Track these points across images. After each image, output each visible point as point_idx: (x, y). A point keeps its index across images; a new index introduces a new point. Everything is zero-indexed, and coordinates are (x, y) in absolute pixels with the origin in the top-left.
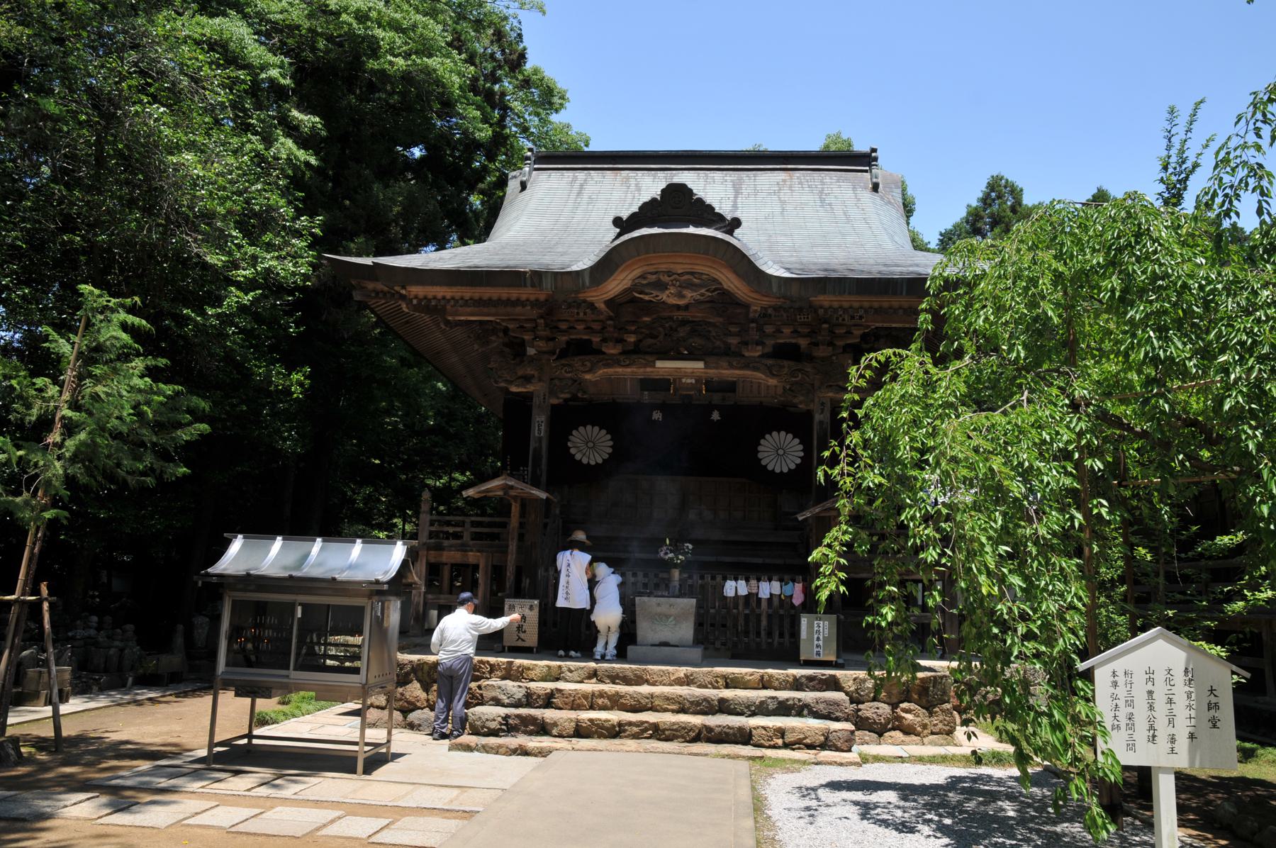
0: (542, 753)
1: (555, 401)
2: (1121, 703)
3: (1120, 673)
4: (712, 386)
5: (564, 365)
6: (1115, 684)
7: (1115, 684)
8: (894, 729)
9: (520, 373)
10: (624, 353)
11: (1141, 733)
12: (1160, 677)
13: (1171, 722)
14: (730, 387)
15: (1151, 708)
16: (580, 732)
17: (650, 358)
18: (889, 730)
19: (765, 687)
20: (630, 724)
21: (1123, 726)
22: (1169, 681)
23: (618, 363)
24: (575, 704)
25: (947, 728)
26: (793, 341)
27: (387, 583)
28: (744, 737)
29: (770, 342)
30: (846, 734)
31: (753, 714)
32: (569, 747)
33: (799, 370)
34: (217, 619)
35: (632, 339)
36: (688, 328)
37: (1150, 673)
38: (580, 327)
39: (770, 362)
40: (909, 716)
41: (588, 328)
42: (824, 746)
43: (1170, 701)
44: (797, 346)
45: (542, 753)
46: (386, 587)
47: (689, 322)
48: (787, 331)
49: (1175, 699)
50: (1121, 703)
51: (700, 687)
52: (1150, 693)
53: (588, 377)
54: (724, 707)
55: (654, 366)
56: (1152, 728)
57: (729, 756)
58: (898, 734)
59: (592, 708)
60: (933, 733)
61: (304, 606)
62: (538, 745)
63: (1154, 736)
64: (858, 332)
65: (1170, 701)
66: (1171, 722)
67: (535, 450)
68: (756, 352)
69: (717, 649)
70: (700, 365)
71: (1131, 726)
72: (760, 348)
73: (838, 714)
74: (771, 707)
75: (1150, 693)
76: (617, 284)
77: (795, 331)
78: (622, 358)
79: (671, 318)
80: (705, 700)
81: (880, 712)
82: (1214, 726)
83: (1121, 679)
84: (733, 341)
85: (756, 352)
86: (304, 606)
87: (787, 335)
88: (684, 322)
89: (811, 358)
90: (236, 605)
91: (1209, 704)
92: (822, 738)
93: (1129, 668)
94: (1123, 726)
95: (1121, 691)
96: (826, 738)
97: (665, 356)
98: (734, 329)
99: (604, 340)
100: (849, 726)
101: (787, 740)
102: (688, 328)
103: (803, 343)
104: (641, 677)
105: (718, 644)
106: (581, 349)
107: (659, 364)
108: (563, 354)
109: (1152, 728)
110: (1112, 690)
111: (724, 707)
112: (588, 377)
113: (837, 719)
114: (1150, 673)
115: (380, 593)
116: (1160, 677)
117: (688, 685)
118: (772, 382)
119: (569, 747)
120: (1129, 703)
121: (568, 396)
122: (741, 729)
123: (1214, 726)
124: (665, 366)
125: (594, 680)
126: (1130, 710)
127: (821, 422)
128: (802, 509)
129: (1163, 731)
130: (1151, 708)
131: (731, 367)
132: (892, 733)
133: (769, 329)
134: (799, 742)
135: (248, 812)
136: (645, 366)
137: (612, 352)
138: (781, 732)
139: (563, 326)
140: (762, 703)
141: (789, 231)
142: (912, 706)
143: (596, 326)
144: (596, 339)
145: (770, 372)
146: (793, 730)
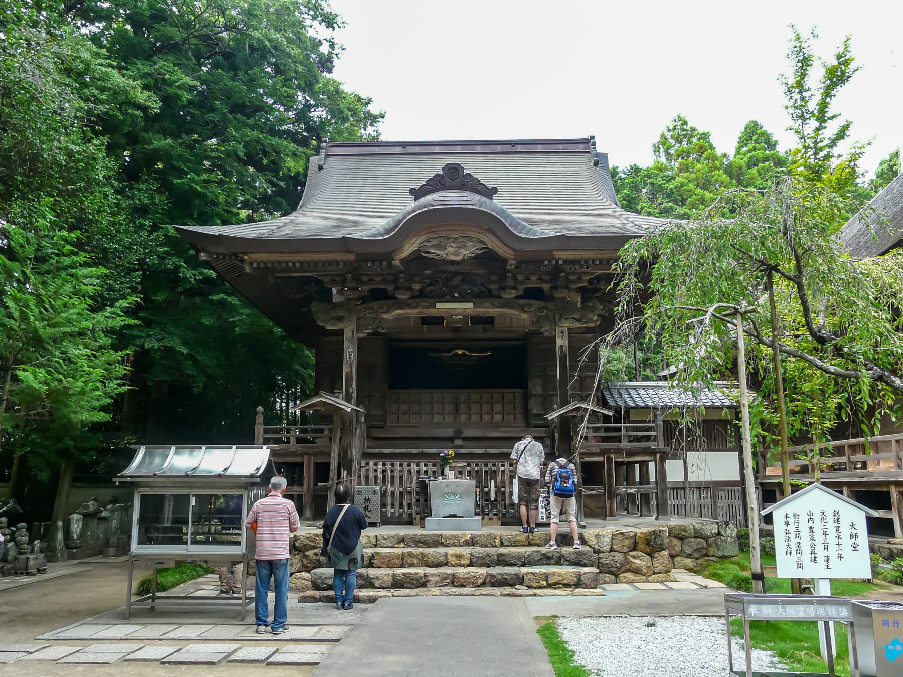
0: (372, 600)
1: (362, 336)
2: (792, 536)
3: (791, 515)
4: (477, 320)
5: (367, 308)
6: (787, 523)
7: (787, 523)
8: (627, 571)
9: (334, 315)
10: (412, 298)
11: (806, 556)
12: (817, 517)
13: (826, 547)
14: (490, 320)
15: (812, 538)
16: (398, 584)
17: (432, 301)
18: (623, 572)
19: (530, 544)
20: (433, 575)
21: (794, 552)
22: (823, 520)
23: (409, 306)
24: (390, 563)
25: (665, 569)
26: (539, 286)
27: (259, 477)
28: (520, 580)
29: (522, 287)
30: (593, 575)
31: (524, 565)
32: (390, 594)
33: (544, 308)
34: (128, 510)
35: (417, 287)
36: (459, 278)
37: (810, 514)
38: (377, 279)
39: (522, 302)
40: (637, 561)
41: (383, 280)
42: (578, 585)
43: (825, 533)
44: (541, 290)
45: (372, 600)
46: (259, 480)
47: (460, 273)
48: (534, 278)
49: (828, 531)
50: (792, 536)
51: (481, 546)
52: (811, 528)
53: (385, 316)
54: (502, 561)
55: (435, 307)
56: (813, 552)
57: (508, 595)
58: (629, 575)
59: (402, 566)
60: (654, 573)
61: (198, 497)
62: (366, 594)
63: (815, 557)
64: (586, 278)
65: (825, 533)
66: (826, 547)
67: (347, 373)
68: (511, 295)
69: (491, 519)
70: (471, 305)
71: (799, 552)
72: (514, 291)
73: (586, 561)
74: (537, 558)
75: (811, 528)
76: (410, 248)
77: (539, 279)
78: (410, 302)
79: (446, 271)
80: (488, 555)
81: (616, 558)
82: (855, 549)
83: (791, 520)
84: (494, 287)
85: (511, 295)
86: (198, 497)
87: (533, 283)
88: (456, 274)
89: (552, 298)
90: (144, 498)
91: (851, 534)
92: (576, 579)
93: (796, 512)
94: (794, 552)
95: (792, 528)
96: (579, 579)
97: (443, 299)
98: (494, 278)
99: (397, 289)
100: (595, 570)
101: (550, 582)
102: (459, 278)
103: (546, 287)
104: (438, 541)
105: (491, 515)
106: (379, 295)
107: (439, 305)
108: (364, 300)
109: (813, 552)
110: (786, 527)
111: (502, 561)
112: (385, 316)
113: (585, 565)
114: (810, 514)
115: (253, 484)
116: (817, 517)
117: (473, 545)
118: (524, 316)
119: (390, 594)
120: (798, 536)
121: (370, 331)
122: (516, 575)
123: (855, 549)
124: (443, 307)
125: (402, 545)
126: (798, 540)
127: (561, 346)
128: (550, 410)
129: (821, 554)
130: (812, 538)
131: (494, 306)
132: (626, 575)
133: (520, 277)
134: (556, 584)
135: (171, 650)
136: (428, 307)
137: (403, 297)
138: (546, 577)
139: (365, 279)
140: (529, 555)
141: (540, 209)
142: (640, 553)
143: (390, 278)
144: (390, 288)
145: (522, 309)
146: (554, 574)
